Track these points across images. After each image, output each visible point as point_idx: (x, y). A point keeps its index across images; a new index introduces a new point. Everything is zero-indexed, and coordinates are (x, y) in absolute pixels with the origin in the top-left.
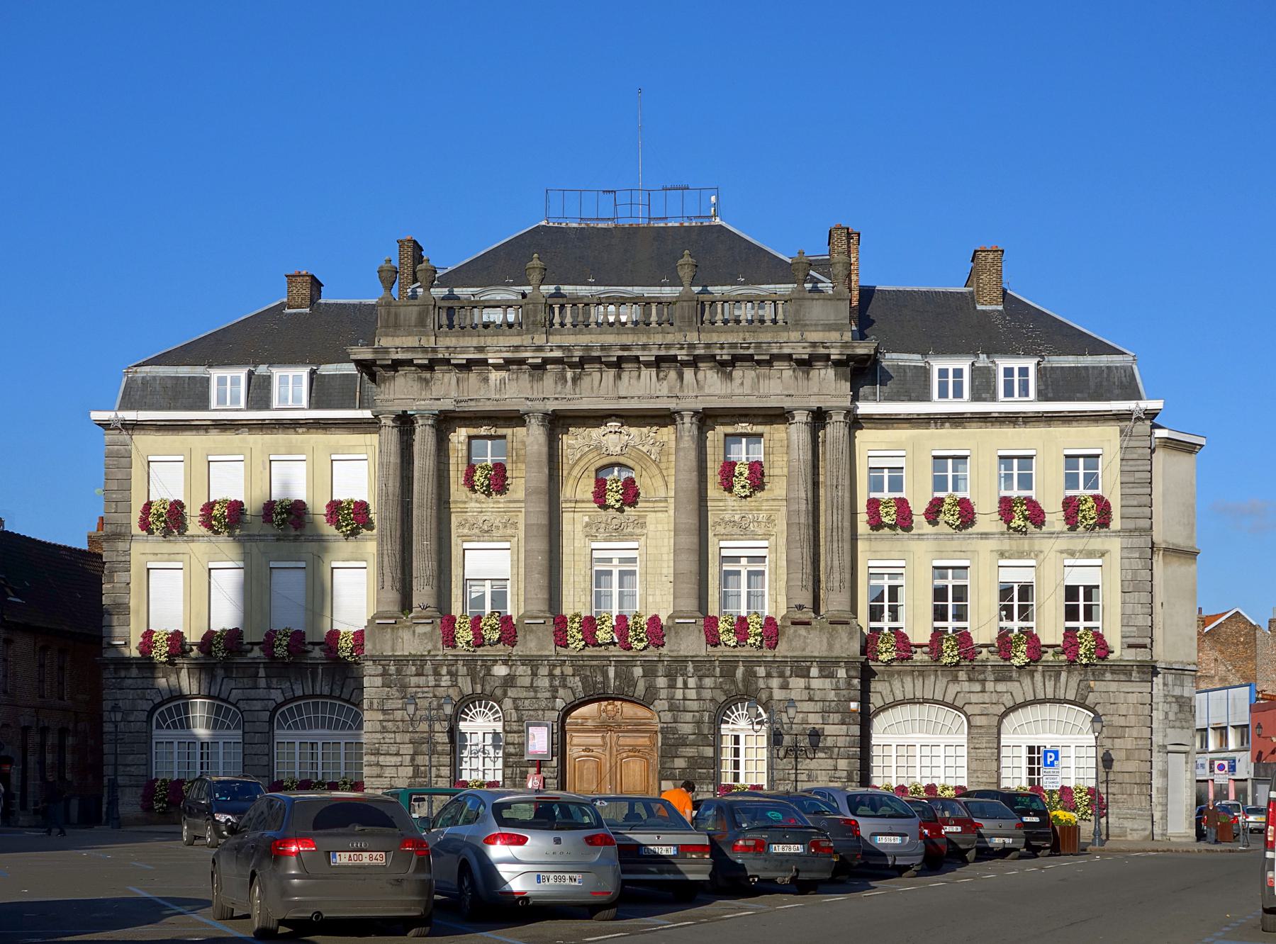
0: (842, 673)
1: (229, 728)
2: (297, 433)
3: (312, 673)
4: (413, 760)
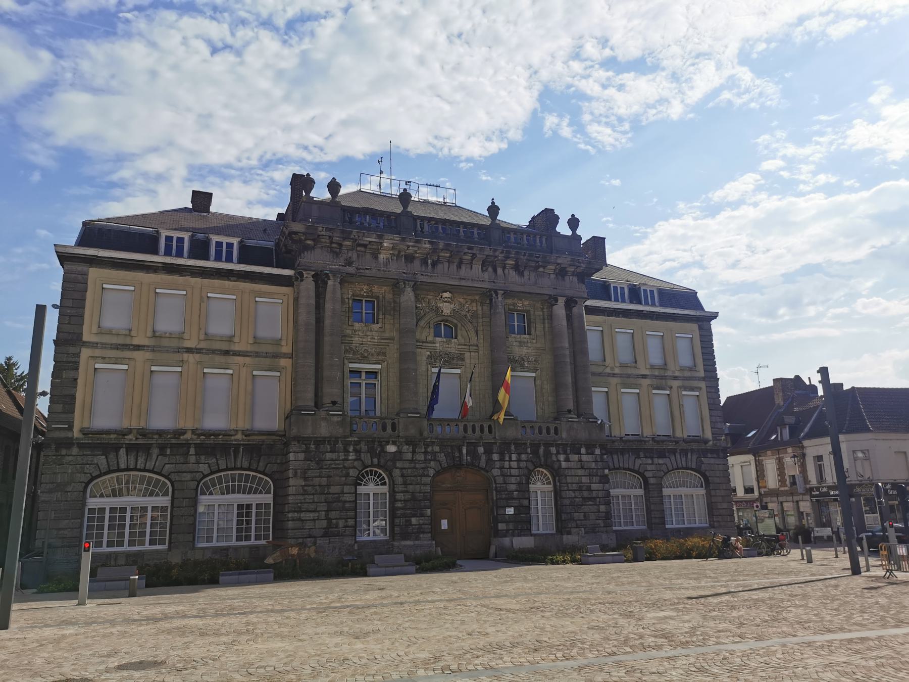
0: (598, 451)
1: (157, 495)
2: (230, 280)
3: (234, 451)
4: (327, 515)
